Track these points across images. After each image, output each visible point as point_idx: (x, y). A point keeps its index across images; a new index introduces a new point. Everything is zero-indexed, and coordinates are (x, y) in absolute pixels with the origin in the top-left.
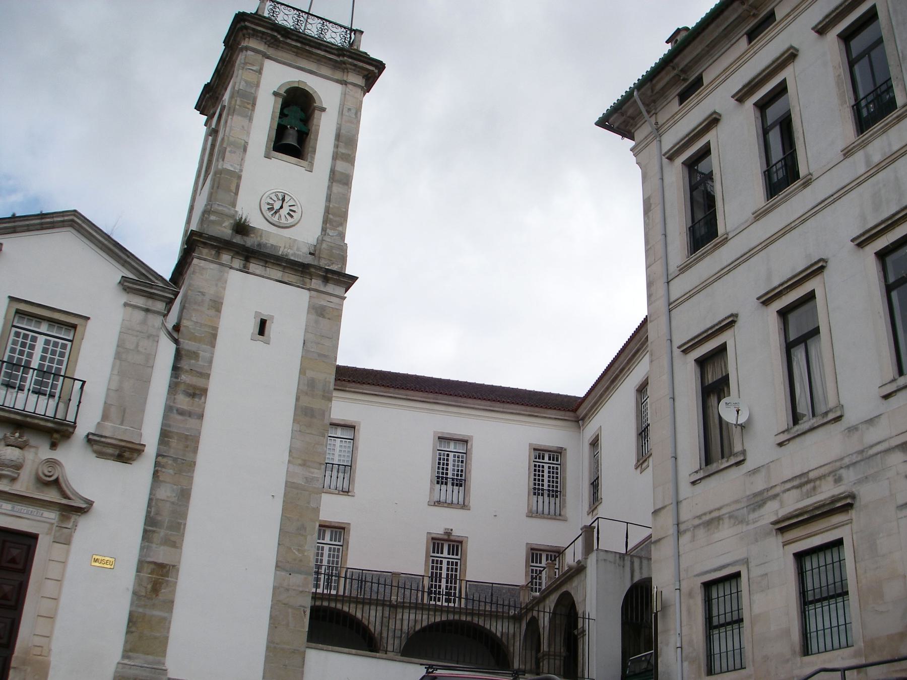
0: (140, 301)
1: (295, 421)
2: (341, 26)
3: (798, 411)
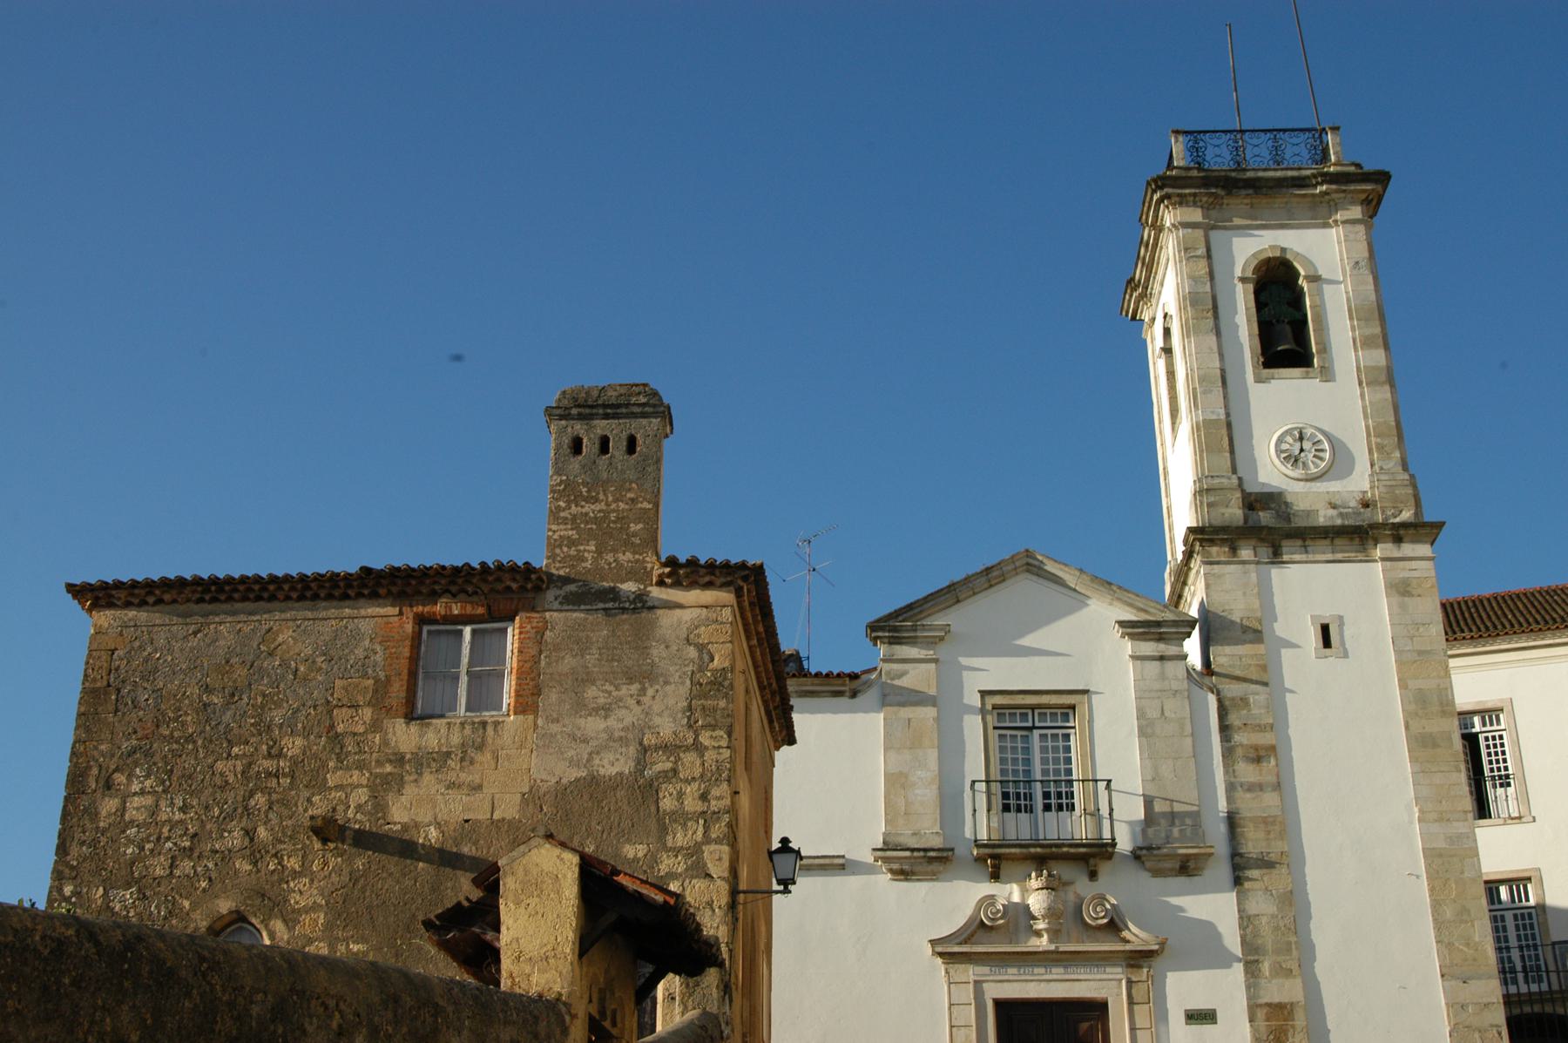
0: (1149, 648)
1: (1413, 759)
2: (1265, 131)
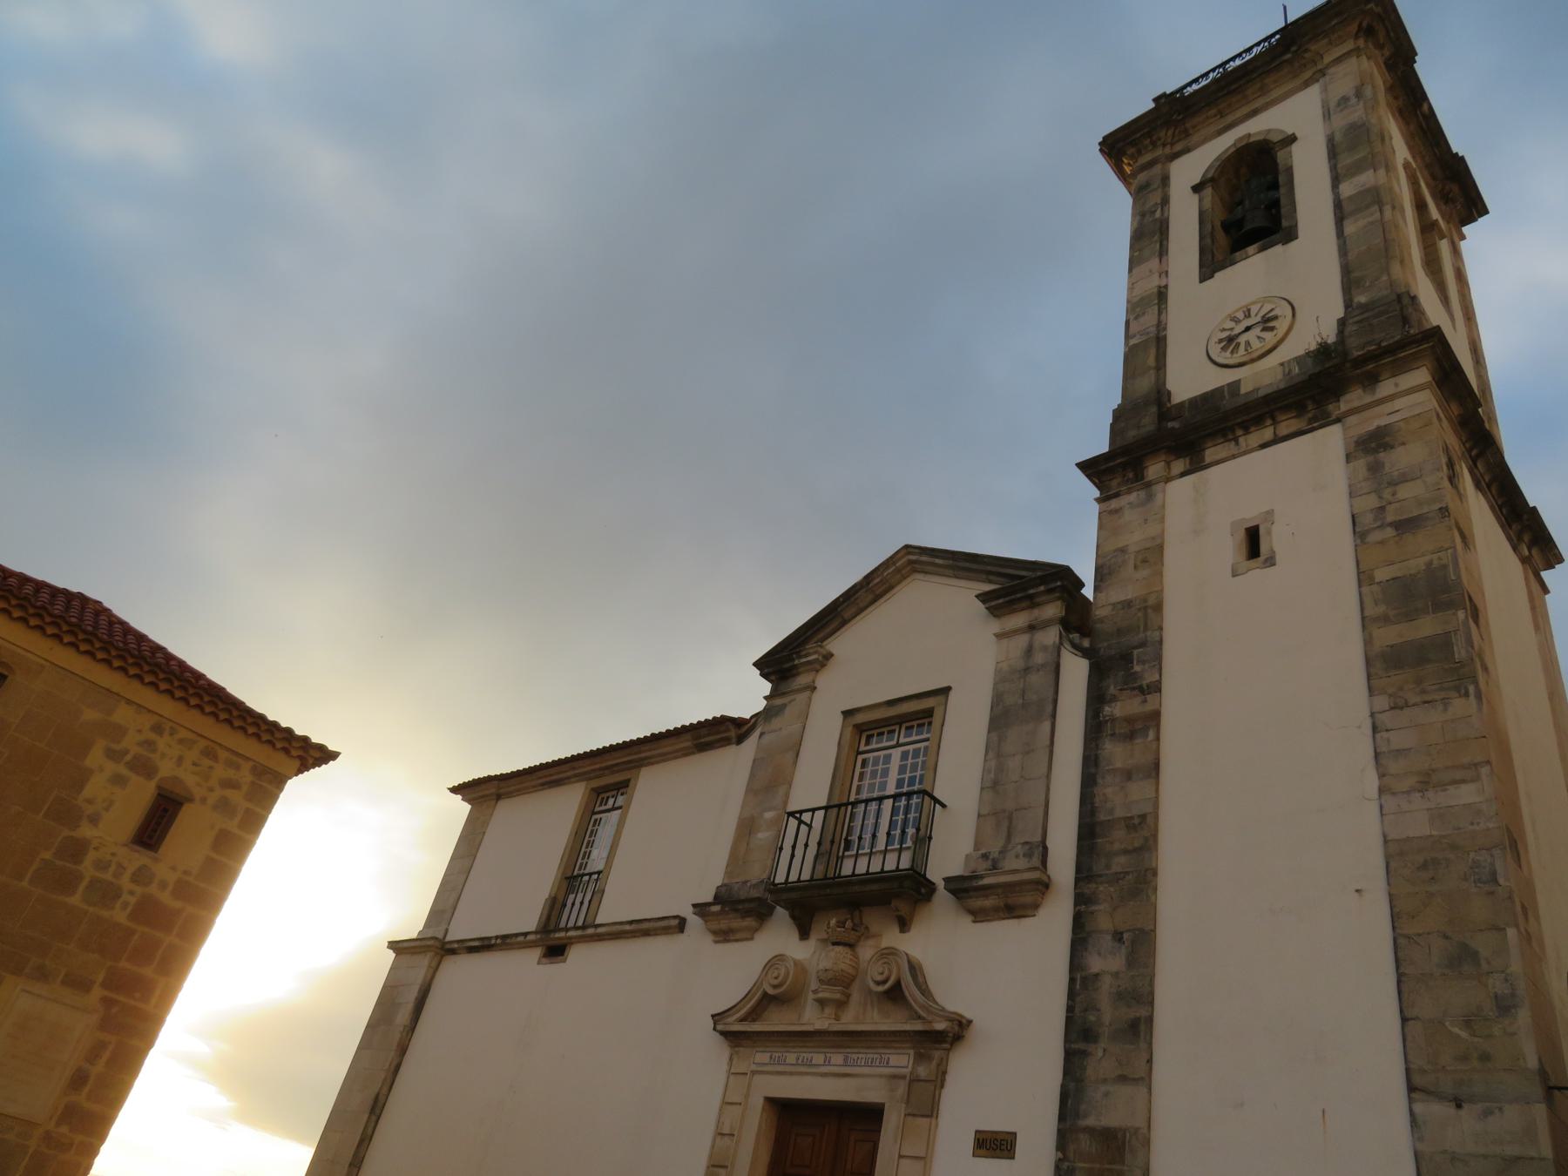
3: (1105, 449)
